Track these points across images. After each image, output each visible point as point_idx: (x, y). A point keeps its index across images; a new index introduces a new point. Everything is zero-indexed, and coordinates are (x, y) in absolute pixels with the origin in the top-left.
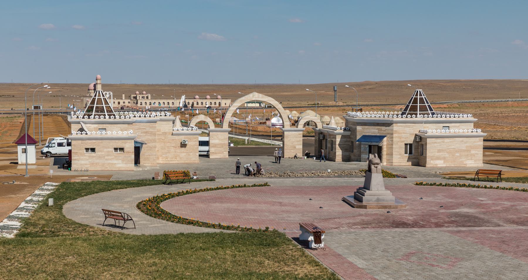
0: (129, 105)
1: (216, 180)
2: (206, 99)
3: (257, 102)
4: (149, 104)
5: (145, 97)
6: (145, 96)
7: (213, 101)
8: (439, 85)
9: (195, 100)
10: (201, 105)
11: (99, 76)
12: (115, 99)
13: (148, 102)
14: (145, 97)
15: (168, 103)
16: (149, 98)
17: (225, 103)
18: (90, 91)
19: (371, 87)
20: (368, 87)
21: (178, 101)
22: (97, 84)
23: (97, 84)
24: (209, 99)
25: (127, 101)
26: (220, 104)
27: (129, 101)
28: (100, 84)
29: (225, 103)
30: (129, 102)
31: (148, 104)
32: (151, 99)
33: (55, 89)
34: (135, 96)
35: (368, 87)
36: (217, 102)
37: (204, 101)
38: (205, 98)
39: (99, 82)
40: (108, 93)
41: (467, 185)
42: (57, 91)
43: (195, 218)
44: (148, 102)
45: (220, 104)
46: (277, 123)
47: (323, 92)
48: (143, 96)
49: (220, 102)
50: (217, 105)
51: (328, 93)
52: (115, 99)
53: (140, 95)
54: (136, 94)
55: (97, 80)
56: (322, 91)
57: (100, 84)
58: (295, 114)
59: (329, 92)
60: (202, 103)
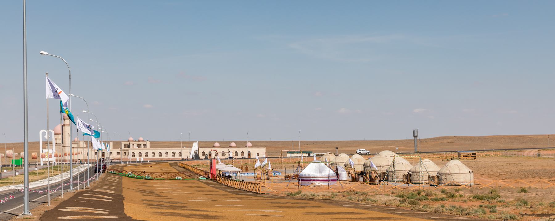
0: (119, 156)
1: (284, 177)
3: (306, 152)
4: (145, 155)
5: (142, 146)
6: (142, 144)
7: (239, 151)
8: (528, 139)
9: (214, 149)
10: (173, 156)
13: (150, 152)
14: (142, 146)
15: (160, 153)
16: (148, 146)
17: (258, 153)
19: (449, 141)
20: (445, 141)
21: (188, 150)
22: (64, 125)
23: (64, 125)
24: (235, 147)
25: (115, 152)
26: (249, 154)
27: (119, 151)
29: (258, 153)
30: (118, 153)
31: (144, 154)
32: (151, 147)
34: (128, 143)
35: (445, 141)
36: (246, 151)
38: (212, 145)
44: (144, 152)
45: (249, 154)
46: (318, 175)
47: (393, 147)
48: (139, 143)
49: (249, 152)
50: (246, 156)
53: (133, 143)
54: (129, 141)
56: (391, 145)
58: (359, 161)
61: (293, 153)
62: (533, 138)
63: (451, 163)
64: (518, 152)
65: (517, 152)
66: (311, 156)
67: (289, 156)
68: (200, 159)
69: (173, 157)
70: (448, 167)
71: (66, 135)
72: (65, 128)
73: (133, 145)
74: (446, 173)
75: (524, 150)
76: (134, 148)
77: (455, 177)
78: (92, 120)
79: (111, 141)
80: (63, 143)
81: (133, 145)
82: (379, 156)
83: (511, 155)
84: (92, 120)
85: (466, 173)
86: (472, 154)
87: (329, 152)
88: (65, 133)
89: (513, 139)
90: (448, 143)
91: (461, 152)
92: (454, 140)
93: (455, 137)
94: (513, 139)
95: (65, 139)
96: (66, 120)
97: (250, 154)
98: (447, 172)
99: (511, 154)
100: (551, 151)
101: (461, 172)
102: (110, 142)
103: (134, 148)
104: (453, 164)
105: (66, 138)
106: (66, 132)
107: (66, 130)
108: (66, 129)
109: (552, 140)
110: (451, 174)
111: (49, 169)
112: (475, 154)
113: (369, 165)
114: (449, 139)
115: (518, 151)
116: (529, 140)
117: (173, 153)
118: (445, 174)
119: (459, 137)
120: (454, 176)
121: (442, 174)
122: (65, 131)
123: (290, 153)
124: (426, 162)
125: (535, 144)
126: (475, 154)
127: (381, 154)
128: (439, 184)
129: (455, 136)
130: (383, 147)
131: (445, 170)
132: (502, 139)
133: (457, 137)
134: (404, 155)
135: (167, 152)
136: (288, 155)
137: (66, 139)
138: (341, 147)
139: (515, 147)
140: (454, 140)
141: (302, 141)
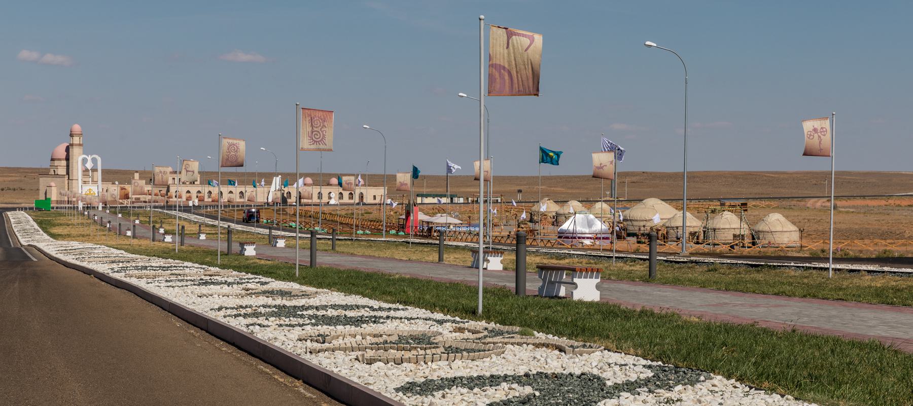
2: (329, 184)
8: (765, 178)
11: (77, 128)
12: (117, 183)
18: (56, 163)
19: (634, 179)
22: (72, 145)
23: (72, 145)
26: (361, 196)
28: (80, 145)
33: (10, 176)
37: (325, 191)
39: (76, 140)
40: (89, 158)
41: (244, 306)
42: (13, 181)
43: (271, 378)
46: (587, 231)
51: (555, 189)
52: (117, 183)
55: (72, 135)
57: (80, 145)
59: (555, 187)
60: (320, 195)
61: (427, 196)
62: (772, 177)
63: (770, 217)
64: (798, 202)
65: (796, 202)
66: (455, 203)
67: (421, 202)
68: (288, 204)
69: (242, 200)
70: (767, 223)
71: (74, 161)
72: (73, 151)
73: (174, 179)
74: (764, 230)
75: (807, 200)
76: (174, 184)
77: (777, 236)
78: (264, 149)
79: (137, 172)
80: (68, 173)
81: (174, 179)
82: (643, 206)
83: (793, 207)
84: (264, 149)
85: (791, 231)
86: (741, 204)
87: (547, 199)
88: (73, 158)
89: (739, 178)
90: (634, 182)
91: (726, 201)
92: (642, 178)
93: (643, 172)
94: (739, 178)
95: (73, 167)
96: (74, 138)
97: (362, 197)
98: (766, 229)
99: (789, 205)
100: (847, 201)
101: (785, 230)
102: (135, 174)
103: (174, 184)
104: (773, 219)
105: (74, 166)
106: (74, 157)
107: (74, 154)
108: (74, 151)
109: (804, 182)
110: (771, 232)
111: (299, 218)
112: (746, 204)
113: (629, 218)
114: (634, 176)
115: (798, 201)
116: (765, 180)
117: (241, 193)
118: (764, 232)
119: (651, 173)
120: (775, 234)
121: (759, 231)
122: (73, 155)
123: (422, 196)
124: (727, 216)
125: (776, 187)
126: (746, 204)
127: (645, 202)
128: (754, 244)
129: (644, 171)
130: (528, 187)
131: (711, 225)
132: (721, 177)
133: (647, 173)
134: (674, 203)
135: (241, 191)
136: (419, 200)
137: (74, 168)
138: (458, 187)
139: (844, 194)
140: (642, 178)
141: (371, 175)
